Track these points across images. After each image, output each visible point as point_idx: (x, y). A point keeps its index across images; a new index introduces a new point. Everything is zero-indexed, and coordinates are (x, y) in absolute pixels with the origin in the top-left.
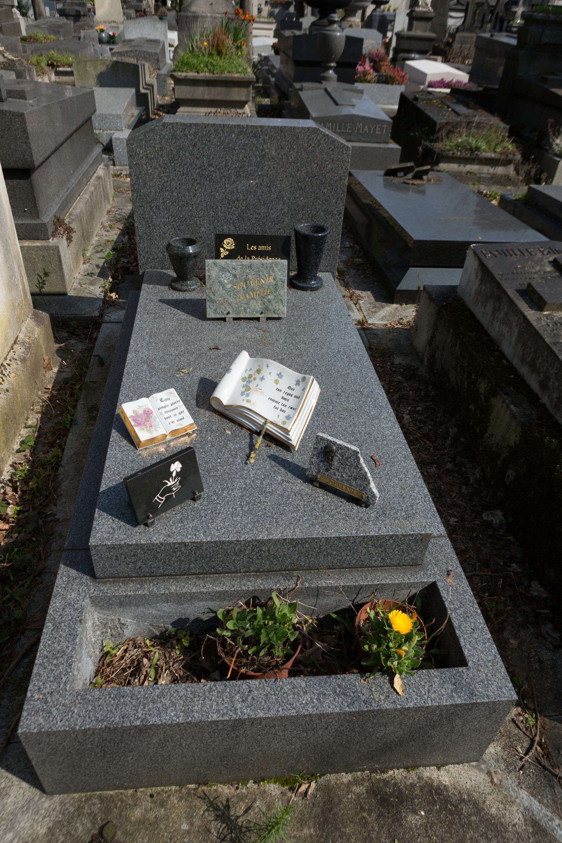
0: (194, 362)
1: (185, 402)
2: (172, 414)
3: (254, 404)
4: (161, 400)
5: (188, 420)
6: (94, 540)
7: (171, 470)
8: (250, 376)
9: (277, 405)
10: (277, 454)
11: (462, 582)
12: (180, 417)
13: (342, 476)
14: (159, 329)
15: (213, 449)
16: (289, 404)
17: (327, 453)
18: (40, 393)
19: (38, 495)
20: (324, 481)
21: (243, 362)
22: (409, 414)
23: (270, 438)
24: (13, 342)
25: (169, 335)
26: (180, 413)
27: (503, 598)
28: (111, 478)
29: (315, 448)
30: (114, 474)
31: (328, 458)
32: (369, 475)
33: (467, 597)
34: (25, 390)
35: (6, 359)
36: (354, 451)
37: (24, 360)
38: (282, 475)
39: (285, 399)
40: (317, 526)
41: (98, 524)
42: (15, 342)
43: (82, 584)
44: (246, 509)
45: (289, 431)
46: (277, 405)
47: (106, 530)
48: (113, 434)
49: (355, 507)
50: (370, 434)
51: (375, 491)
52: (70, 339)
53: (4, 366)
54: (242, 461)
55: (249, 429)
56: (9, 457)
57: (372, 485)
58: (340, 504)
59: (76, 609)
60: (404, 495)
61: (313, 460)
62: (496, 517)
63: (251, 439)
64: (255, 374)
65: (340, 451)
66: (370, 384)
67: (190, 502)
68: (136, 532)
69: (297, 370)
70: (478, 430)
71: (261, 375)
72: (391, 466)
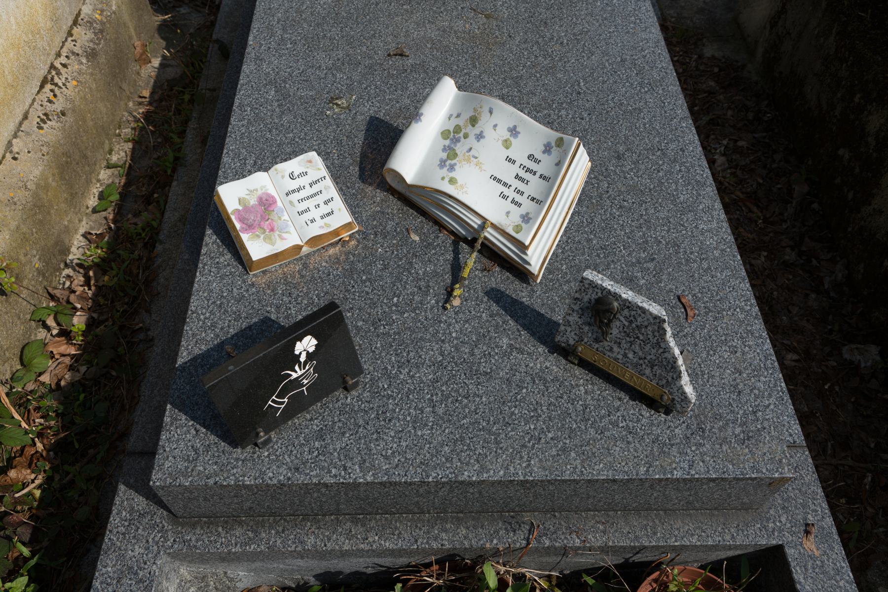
0: (360, 83)
1: (336, 178)
2: (311, 203)
3: (462, 187)
4: (292, 177)
5: (342, 216)
6: (160, 475)
7: (297, 352)
8: (457, 129)
9: (506, 191)
10: (502, 287)
11: (832, 549)
12: (325, 209)
13: (625, 355)
14: (299, 12)
15: (386, 274)
16: (529, 190)
17: (600, 310)
18: (131, 104)
19: (121, 294)
20: (589, 357)
21: (445, 97)
22: (724, 155)
23: (490, 253)
24: (70, 23)
25: (318, 25)
26: (326, 203)
27: (870, 510)
28: (198, 337)
29: (576, 299)
30: (204, 328)
31: (601, 322)
32: (680, 361)
33: (842, 583)
34: (101, 105)
35: (58, 55)
36: (656, 318)
37: (92, 55)
38: (510, 335)
39: (522, 180)
40: (573, 454)
41: (168, 440)
42: (75, 23)
43: (153, 527)
44: (440, 411)
45: (527, 248)
46: (506, 191)
47: (183, 449)
48: (207, 239)
49: (646, 412)
50: (676, 245)
51: (689, 390)
52: (180, 6)
53: (55, 68)
54: (437, 302)
55: (452, 233)
56: (80, 221)
57: (685, 379)
58: (617, 403)
59: (141, 581)
60: (741, 386)
61: (570, 318)
62: (867, 356)
63: (456, 252)
64: (466, 126)
65: (626, 312)
66: (678, 133)
67: (340, 393)
68: (237, 460)
69: (549, 124)
70: (850, 195)
71: (477, 130)
72: (716, 319)
